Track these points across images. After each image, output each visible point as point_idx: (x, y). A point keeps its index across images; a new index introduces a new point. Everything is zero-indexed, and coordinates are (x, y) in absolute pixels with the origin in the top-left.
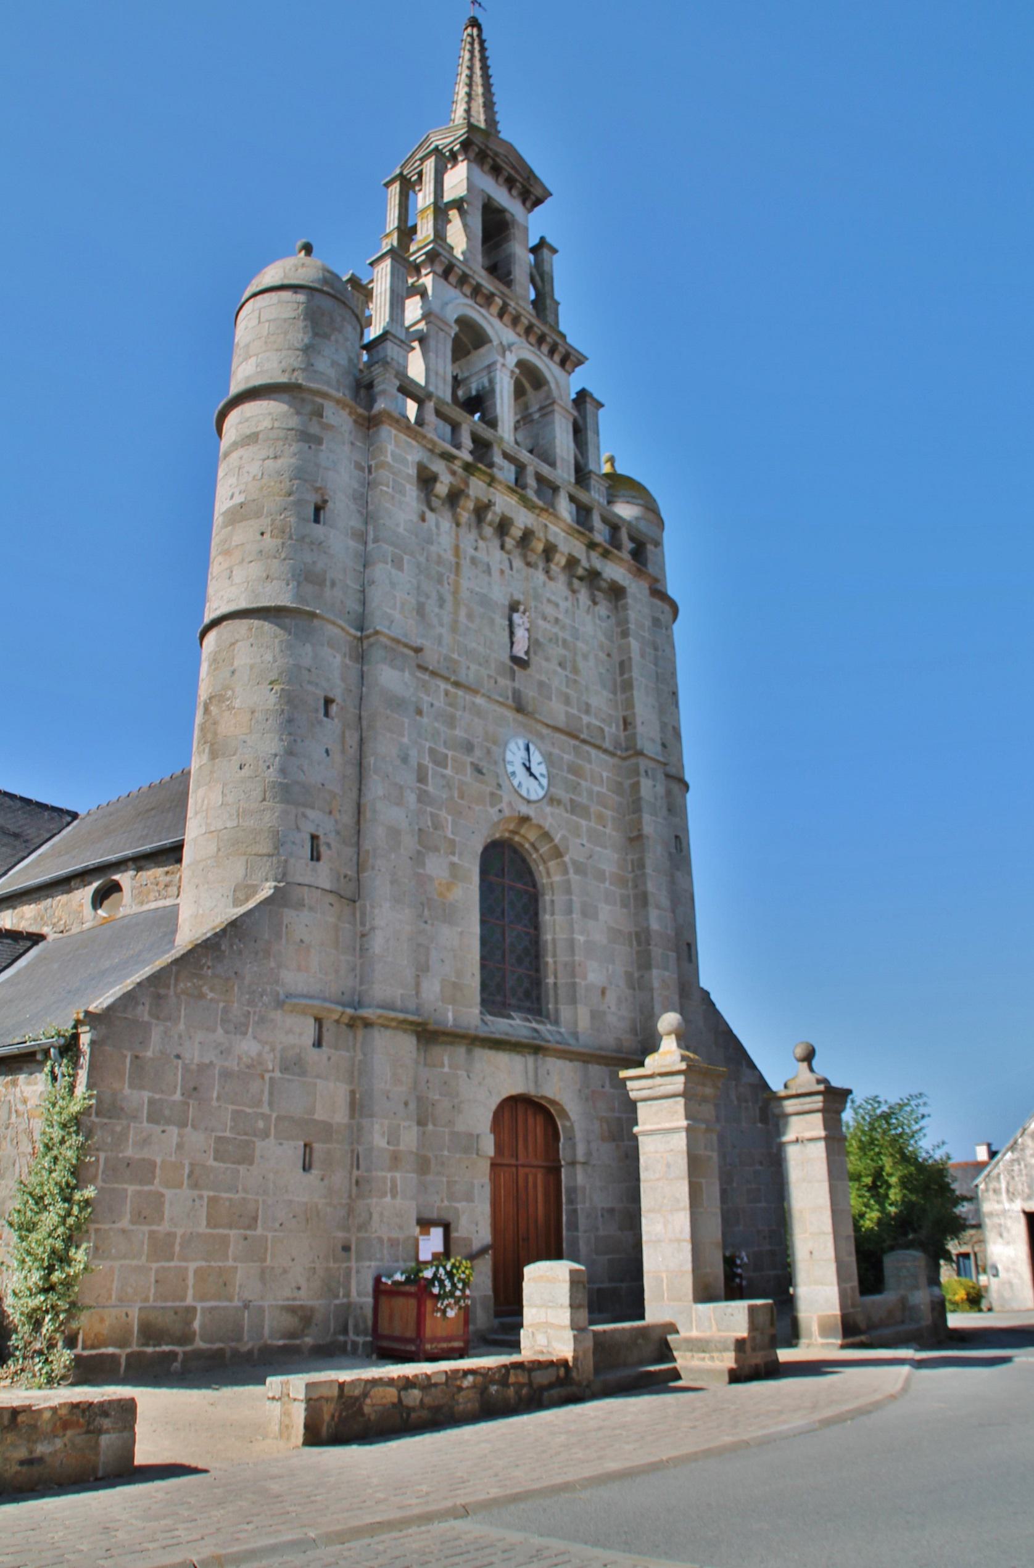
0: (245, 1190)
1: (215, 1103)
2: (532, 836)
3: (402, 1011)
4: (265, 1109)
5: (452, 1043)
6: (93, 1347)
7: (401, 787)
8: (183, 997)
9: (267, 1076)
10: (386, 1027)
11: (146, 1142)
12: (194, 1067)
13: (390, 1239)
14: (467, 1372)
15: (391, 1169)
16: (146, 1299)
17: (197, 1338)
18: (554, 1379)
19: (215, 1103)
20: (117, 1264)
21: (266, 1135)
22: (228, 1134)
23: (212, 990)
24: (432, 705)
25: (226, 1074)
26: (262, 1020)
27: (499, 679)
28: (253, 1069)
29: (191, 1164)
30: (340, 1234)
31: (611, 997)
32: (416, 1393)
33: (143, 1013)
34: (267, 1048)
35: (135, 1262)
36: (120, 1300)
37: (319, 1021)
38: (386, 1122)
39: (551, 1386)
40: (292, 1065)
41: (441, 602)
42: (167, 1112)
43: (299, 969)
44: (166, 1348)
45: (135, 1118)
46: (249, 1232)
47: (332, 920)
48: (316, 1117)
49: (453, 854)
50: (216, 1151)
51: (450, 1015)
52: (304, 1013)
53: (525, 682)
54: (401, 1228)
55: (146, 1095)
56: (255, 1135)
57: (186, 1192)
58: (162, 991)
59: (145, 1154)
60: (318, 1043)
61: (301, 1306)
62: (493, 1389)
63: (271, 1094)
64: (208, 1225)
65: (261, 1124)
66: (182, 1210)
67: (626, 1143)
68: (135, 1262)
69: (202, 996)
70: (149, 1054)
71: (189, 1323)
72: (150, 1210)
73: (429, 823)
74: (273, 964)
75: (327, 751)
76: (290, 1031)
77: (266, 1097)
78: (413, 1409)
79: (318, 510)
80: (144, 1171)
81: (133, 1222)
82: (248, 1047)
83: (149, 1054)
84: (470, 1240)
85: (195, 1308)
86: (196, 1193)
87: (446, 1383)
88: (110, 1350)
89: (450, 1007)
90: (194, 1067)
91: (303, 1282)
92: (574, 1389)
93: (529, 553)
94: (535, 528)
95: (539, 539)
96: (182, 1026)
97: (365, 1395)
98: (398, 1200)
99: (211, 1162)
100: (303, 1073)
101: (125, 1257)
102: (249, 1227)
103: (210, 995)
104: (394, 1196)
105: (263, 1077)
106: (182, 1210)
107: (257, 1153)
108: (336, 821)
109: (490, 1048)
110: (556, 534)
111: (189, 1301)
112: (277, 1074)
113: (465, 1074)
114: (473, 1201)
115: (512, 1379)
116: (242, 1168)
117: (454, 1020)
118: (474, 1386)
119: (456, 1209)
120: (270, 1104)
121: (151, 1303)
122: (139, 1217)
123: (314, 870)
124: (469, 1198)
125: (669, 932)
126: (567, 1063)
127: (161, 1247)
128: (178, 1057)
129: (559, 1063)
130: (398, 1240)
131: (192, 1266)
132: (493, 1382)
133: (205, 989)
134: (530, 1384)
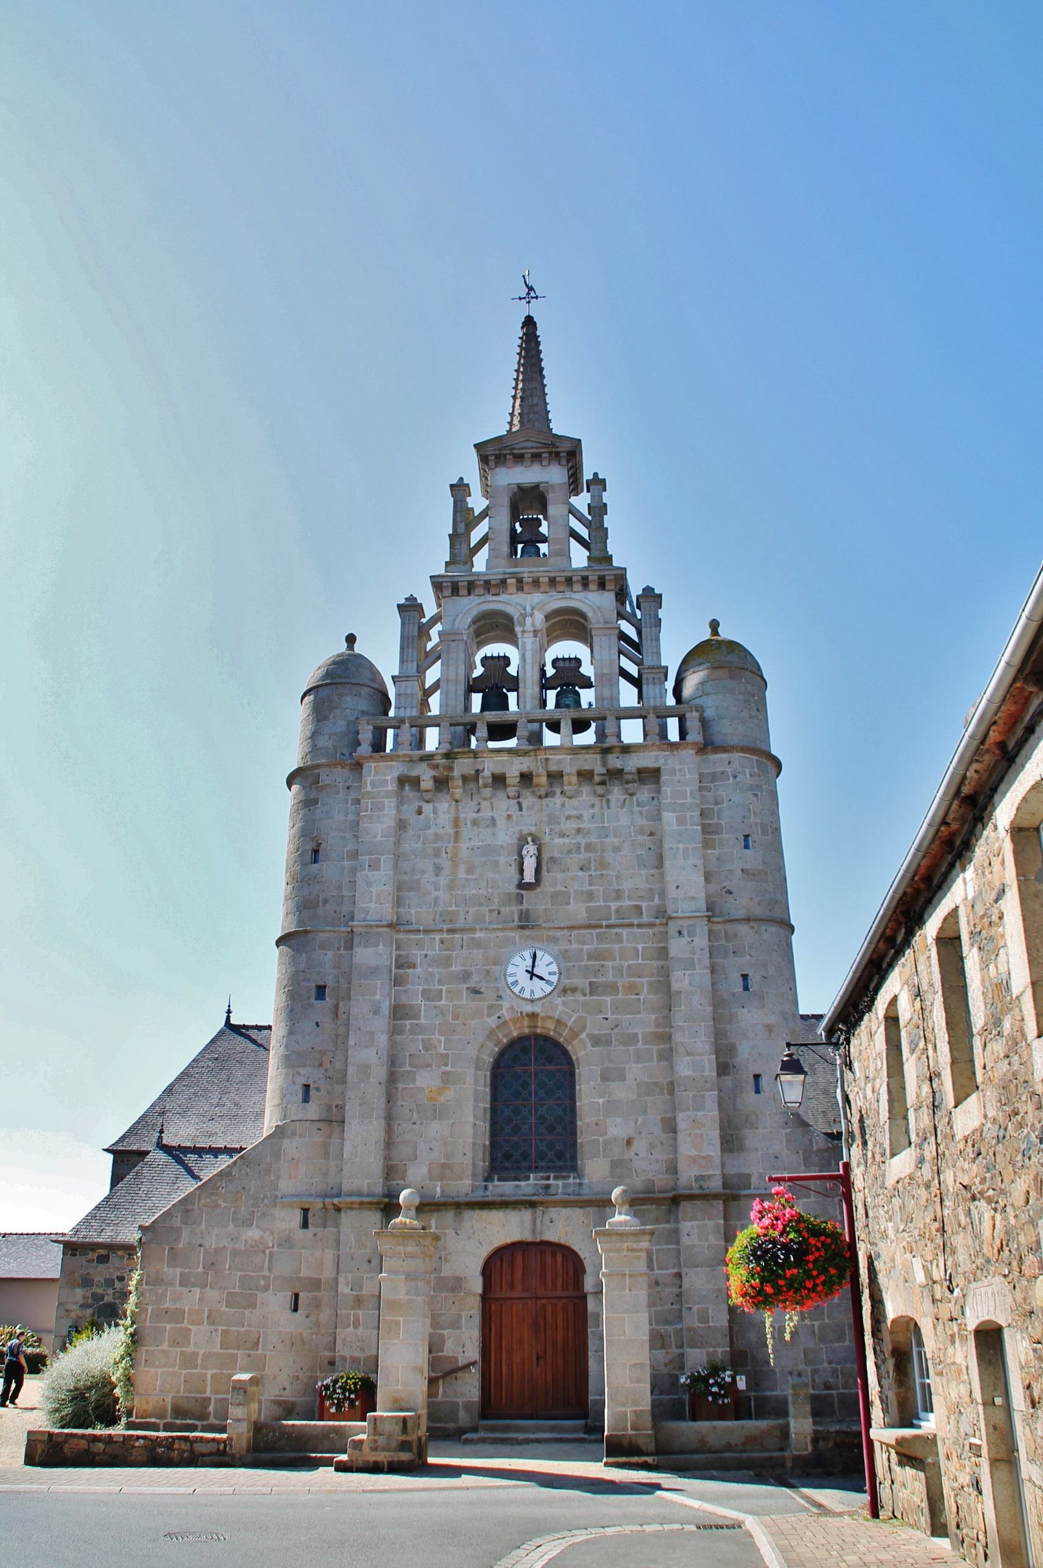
0: (249, 1325)
1: (227, 1272)
2: (551, 1025)
3: (368, 1195)
4: (267, 1273)
5: (439, 1210)
6: (142, 1418)
7: (372, 1033)
8: (204, 1209)
9: (267, 1252)
10: (351, 1209)
11: (179, 1298)
12: (212, 1251)
13: (351, 1357)
14: (138, 1437)
15: (353, 1309)
16: (179, 1391)
17: (212, 1417)
18: (214, 1450)
19: (227, 1272)
20: (160, 1370)
21: (266, 1288)
22: (237, 1290)
23: (224, 1201)
24: (426, 956)
25: (235, 1253)
26: (264, 1215)
27: (502, 909)
28: (257, 1247)
29: (209, 1310)
30: (328, 1354)
31: (640, 1146)
32: (101, 1446)
33: (177, 1222)
34: (268, 1233)
35: (171, 1370)
36: (161, 1391)
37: (306, 1211)
38: (350, 1275)
39: (211, 1454)
40: (287, 1242)
41: (438, 870)
42: (193, 1280)
43: (290, 1178)
44: (190, 1422)
45: (171, 1284)
46: (251, 1352)
47: (318, 1139)
48: (301, 1275)
49: (446, 1065)
50: (227, 1302)
51: (438, 1189)
52: (291, 1206)
53: (533, 901)
54: (362, 1349)
55: (178, 1270)
56: (257, 1290)
57: (205, 1327)
58: (190, 1207)
59: (178, 1305)
60: (305, 1225)
61: (285, 1401)
62: (160, 1450)
63: (270, 1262)
64: (221, 1347)
65: (262, 1283)
66: (203, 1339)
67: (656, 1271)
68: (171, 1370)
69: (217, 1206)
70: (181, 1246)
71: (207, 1407)
72: (181, 1338)
73: (421, 1048)
74: (273, 1178)
75: (317, 1024)
76: (283, 1220)
77: (266, 1265)
78: (99, 1454)
79: (316, 852)
80: (177, 1315)
81: (169, 1346)
82: (253, 1234)
83: (181, 1246)
84: (456, 1358)
85: (210, 1399)
86: (213, 1327)
87: (123, 1442)
88: (153, 1420)
89: (439, 1183)
90: (212, 1251)
91: (287, 1385)
92: (227, 1459)
93: (536, 789)
94: (533, 768)
95: (538, 775)
96: (203, 1227)
97: (66, 1442)
98: (360, 1330)
99: (224, 1308)
100: (291, 1247)
101: (164, 1366)
102: (252, 1349)
103: (224, 1205)
104: (355, 1327)
105: (264, 1252)
106: (203, 1339)
107: (259, 1301)
108: (326, 1070)
109: (481, 1209)
110: (560, 761)
111: (208, 1394)
112: (276, 1249)
113: (453, 1232)
114: (459, 1328)
115: (176, 1446)
116: (247, 1312)
117: (442, 1192)
118: (145, 1446)
119: (442, 1335)
120: (270, 1269)
121: (181, 1394)
122: (174, 1343)
123: (305, 1109)
124: (455, 1325)
125: (707, 1073)
126: (577, 1210)
127: (189, 1361)
128: (201, 1245)
129: (565, 1212)
130: (359, 1359)
131: (210, 1373)
132: (160, 1446)
133: (220, 1202)
134: (192, 1451)
